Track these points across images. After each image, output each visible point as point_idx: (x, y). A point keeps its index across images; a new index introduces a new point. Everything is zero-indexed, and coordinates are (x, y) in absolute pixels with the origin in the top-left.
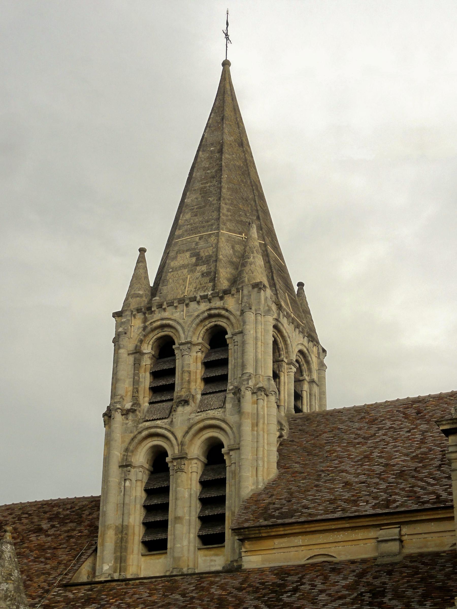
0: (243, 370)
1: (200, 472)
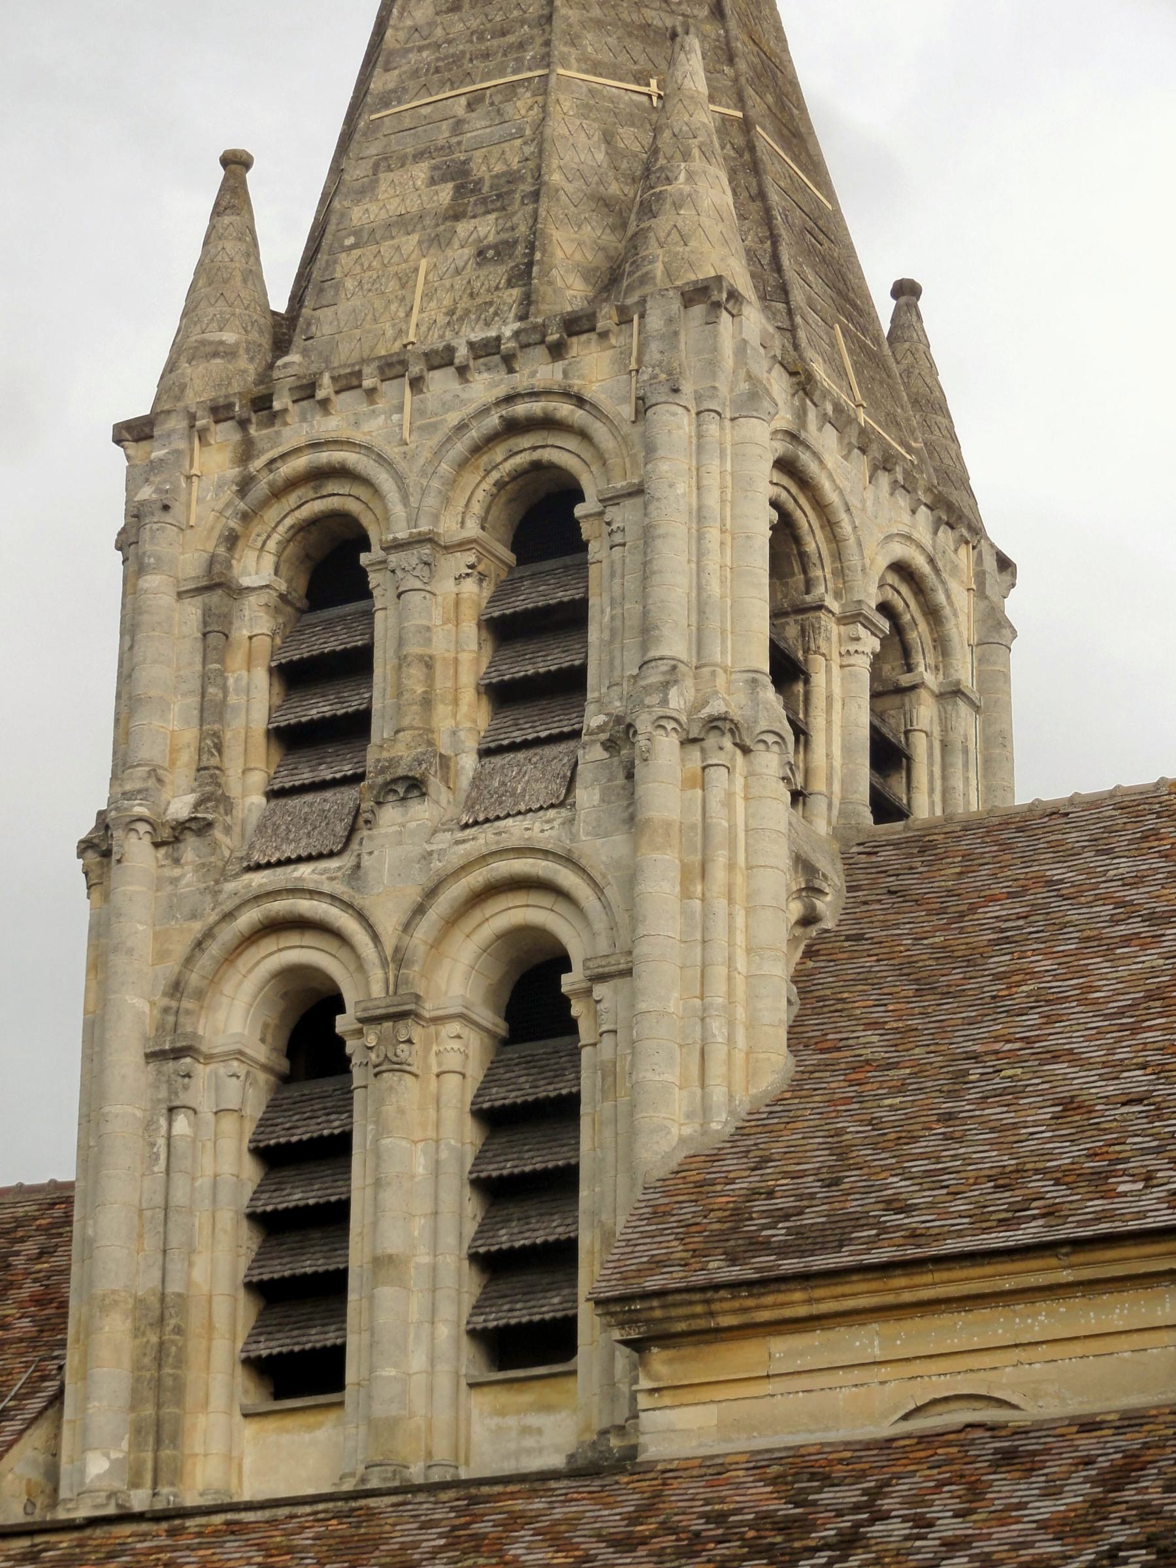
0: (644, 647)
1: (476, 1072)
